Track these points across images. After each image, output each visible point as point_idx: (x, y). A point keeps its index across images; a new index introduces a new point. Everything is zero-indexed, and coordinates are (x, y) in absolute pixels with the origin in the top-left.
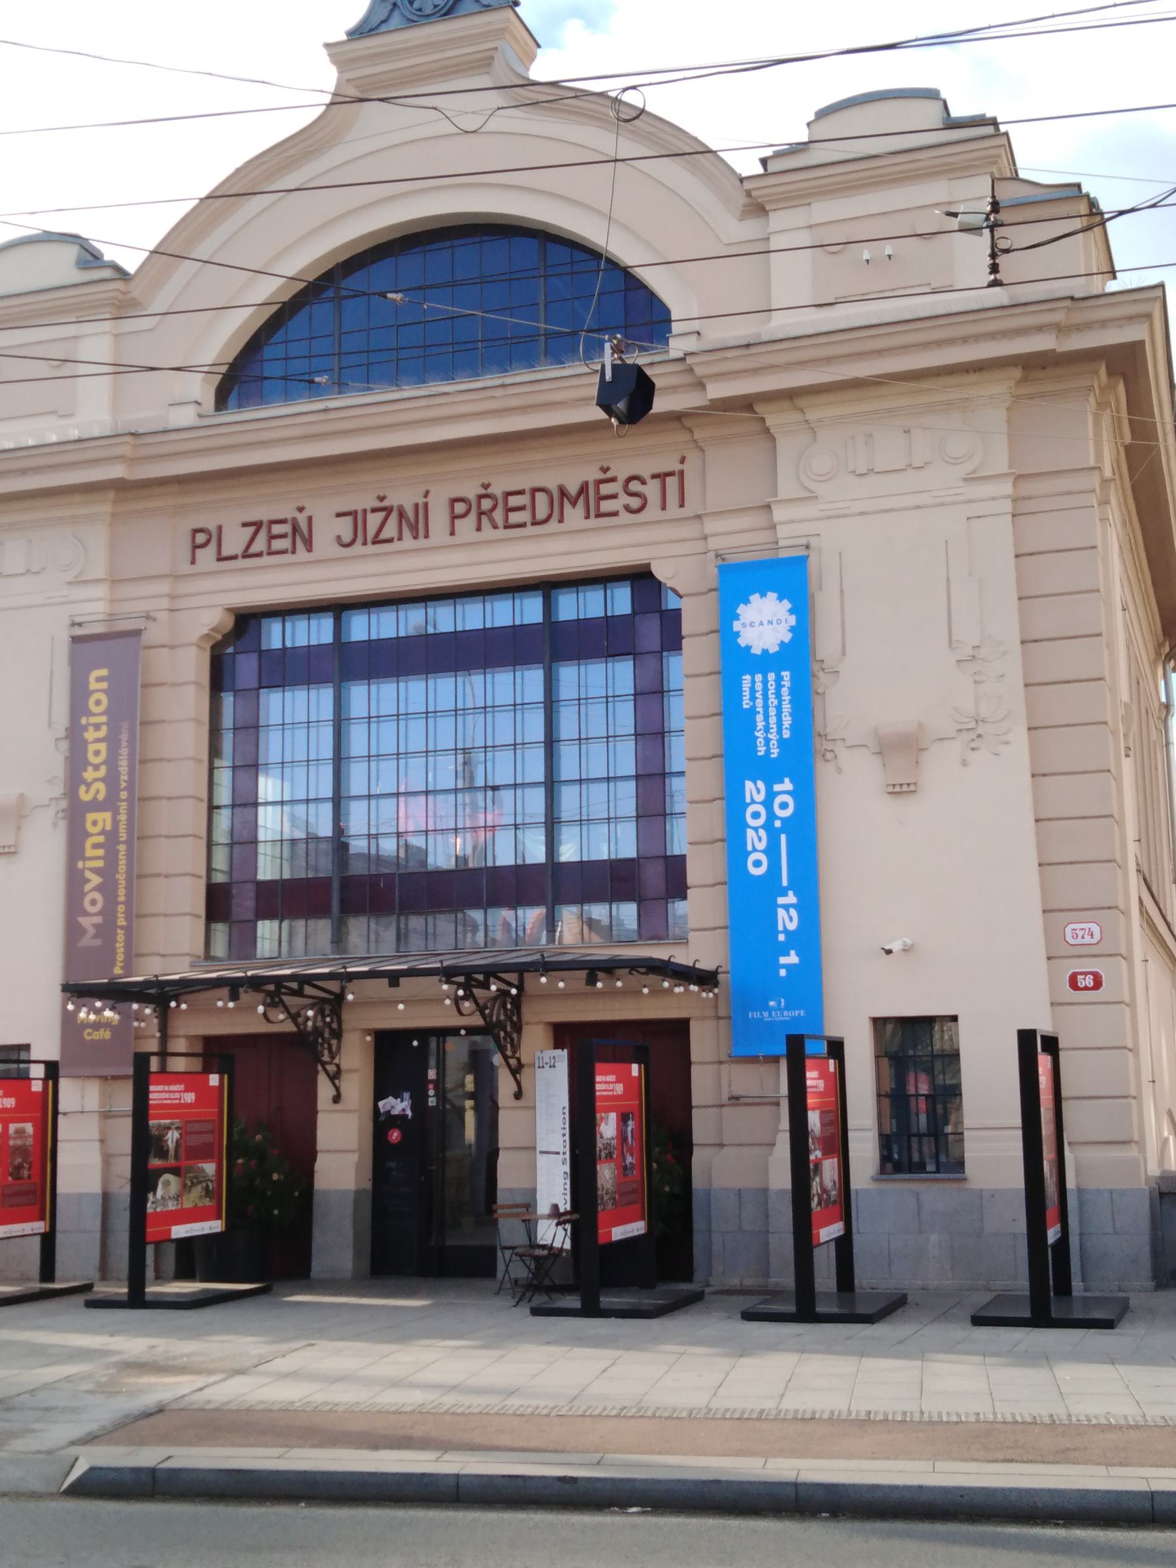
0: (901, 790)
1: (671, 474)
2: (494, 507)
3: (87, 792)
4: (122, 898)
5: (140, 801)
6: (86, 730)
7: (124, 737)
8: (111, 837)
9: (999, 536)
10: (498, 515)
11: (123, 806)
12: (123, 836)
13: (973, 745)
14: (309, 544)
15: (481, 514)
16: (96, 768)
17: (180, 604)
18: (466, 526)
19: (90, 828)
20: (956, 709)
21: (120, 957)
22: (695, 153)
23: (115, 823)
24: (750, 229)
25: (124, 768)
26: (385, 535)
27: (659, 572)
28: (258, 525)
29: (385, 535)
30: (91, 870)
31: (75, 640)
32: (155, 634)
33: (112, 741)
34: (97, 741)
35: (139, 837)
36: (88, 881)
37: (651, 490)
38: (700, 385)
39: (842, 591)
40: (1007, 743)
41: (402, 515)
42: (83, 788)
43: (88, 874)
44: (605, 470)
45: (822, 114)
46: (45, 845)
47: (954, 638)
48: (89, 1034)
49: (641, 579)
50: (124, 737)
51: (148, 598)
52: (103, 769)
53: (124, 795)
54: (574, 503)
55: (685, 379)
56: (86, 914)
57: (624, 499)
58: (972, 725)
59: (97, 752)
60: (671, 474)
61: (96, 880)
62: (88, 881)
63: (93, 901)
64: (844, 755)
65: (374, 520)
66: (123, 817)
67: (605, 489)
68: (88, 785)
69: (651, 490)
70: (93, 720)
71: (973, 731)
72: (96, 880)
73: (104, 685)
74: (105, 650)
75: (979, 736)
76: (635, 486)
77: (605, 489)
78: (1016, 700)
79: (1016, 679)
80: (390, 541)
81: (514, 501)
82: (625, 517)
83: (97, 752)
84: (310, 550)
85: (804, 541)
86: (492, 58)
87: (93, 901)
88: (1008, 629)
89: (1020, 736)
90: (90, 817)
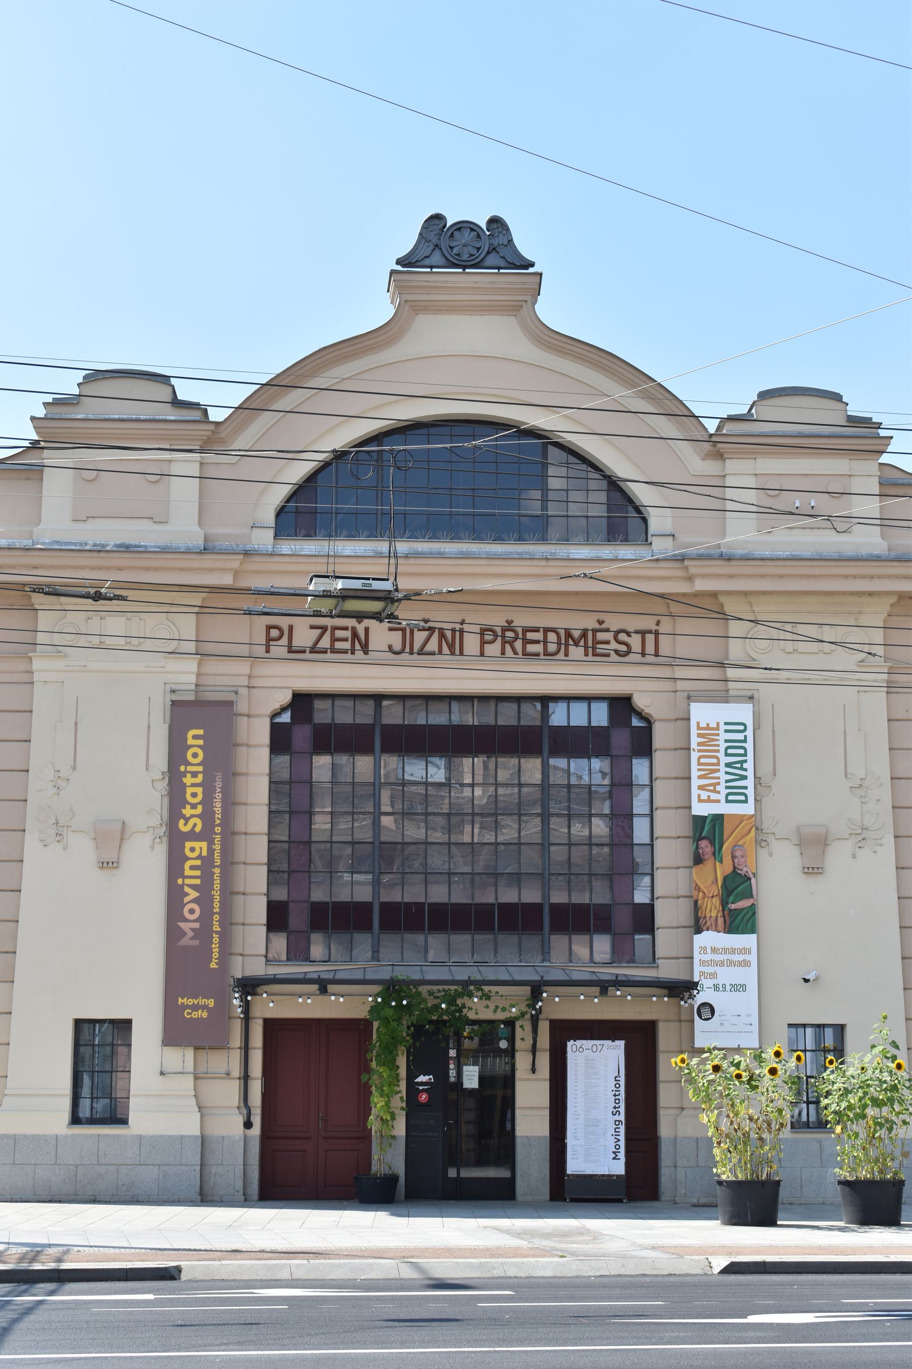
0: (813, 870)
1: (650, 632)
2: (516, 638)
3: (185, 825)
4: (217, 910)
5: (230, 835)
6: (185, 776)
7: (219, 784)
8: (207, 863)
9: (877, 703)
10: (518, 645)
11: (218, 838)
12: (218, 862)
13: (860, 845)
14: (365, 649)
15: (504, 643)
16: (194, 806)
17: (255, 682)
18: (494, 649)
19: (188, 853)
20: (849, 819)
21: (216, 955)
22: (680, 413)
23: (211, 851)
24: (710, 467)
25: (218, 809)
26: (428, 648)
27: (640, 702)
28: (324, 629)
29: (428, 648)
30: (189, 886)
31: (174, 703)
32: (242, 706)
33: (208, 786)
34: (193, 785)
35: (229, 862)
36: (188, 894)
37: (635, 642)
38: (690, 579)
39: (774, 731)
40: (881, 845)
41: (442, 635)
42: (182, 822)
43: (187, 889)
44: (601, 622)
45: (764, 395)
46: (147, 863)
47: (849, 771)
48: (188, 1013)
49: (621, 706)
50: (219, 784)
51: (227, 675)
52: (200, 808)
53: (218, 830)
54: (576, 644)
55: (680, 573)
56: (186, 920)
57: (614, 645)
58: (860, 831)
59: (194, 793)
60: (650, 632)
61: (194, 894)
62: (188, 894)
63: (192, 910)
64: (774, 844)
65: (420, 637)
66: (217, 847)
67: (601, 636)
68: (187, 820)
69: (635, 642)
70: (190, 768)
71: (862, 836)
72: (194, 894)
73: (201, 742)
74: (198, 716)
75: (864, 839)
76: (622, 637)
77: (601, 636)
78: (888, 817)
79: (888, 802)
80: (433, 654)
81: (530, 636)
82: (614, 657)
83: (194, 793)
84: (366, 652)
85: (235, 689)
86: (522, 306)
87: (192, 910)
88: (884, 771)
89: (889, 840)
90: (188, 845)
